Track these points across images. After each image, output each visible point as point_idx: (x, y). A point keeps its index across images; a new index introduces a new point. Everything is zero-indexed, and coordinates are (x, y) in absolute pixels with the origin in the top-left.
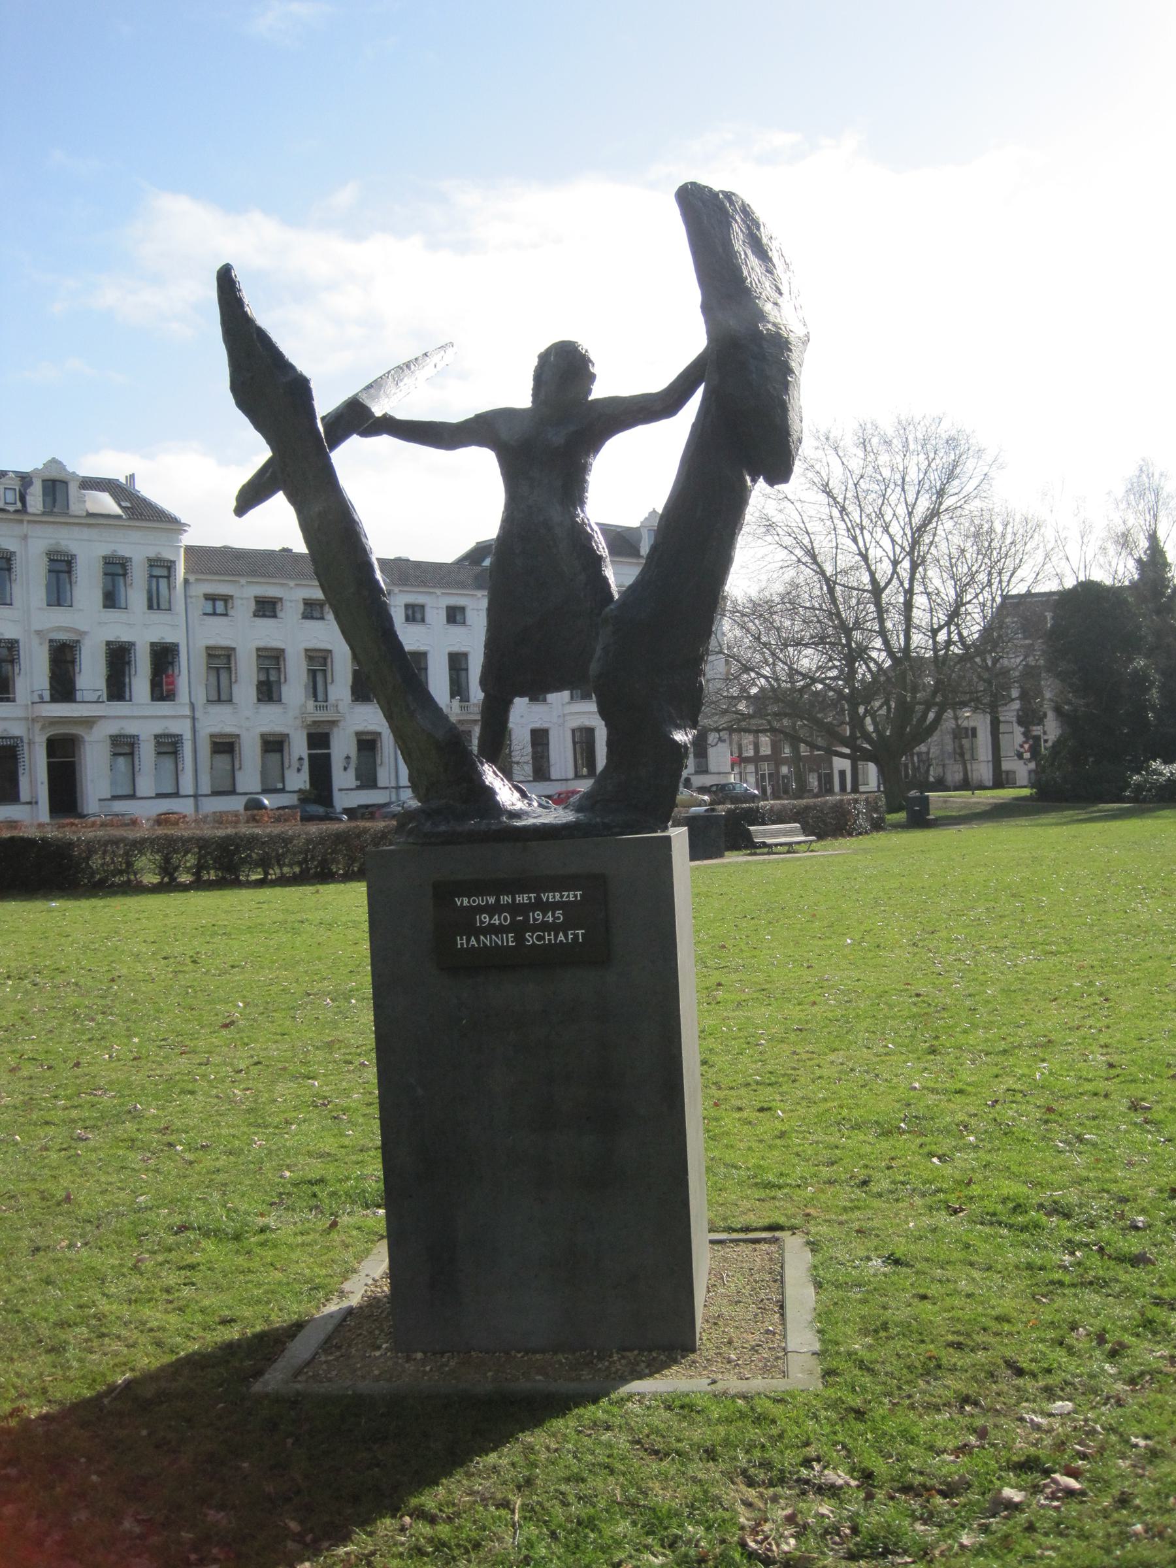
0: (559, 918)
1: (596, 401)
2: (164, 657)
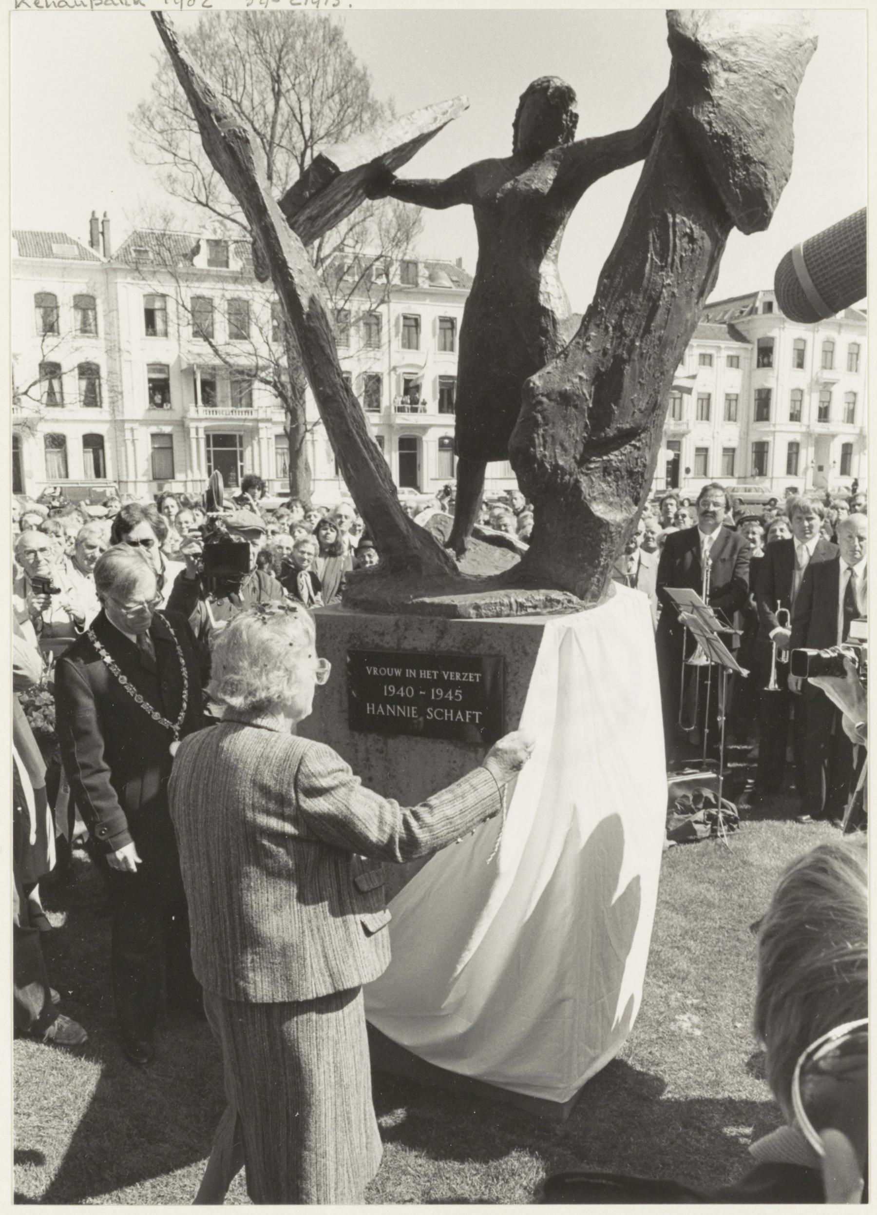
0: (458, 697)
1: (581, 143)
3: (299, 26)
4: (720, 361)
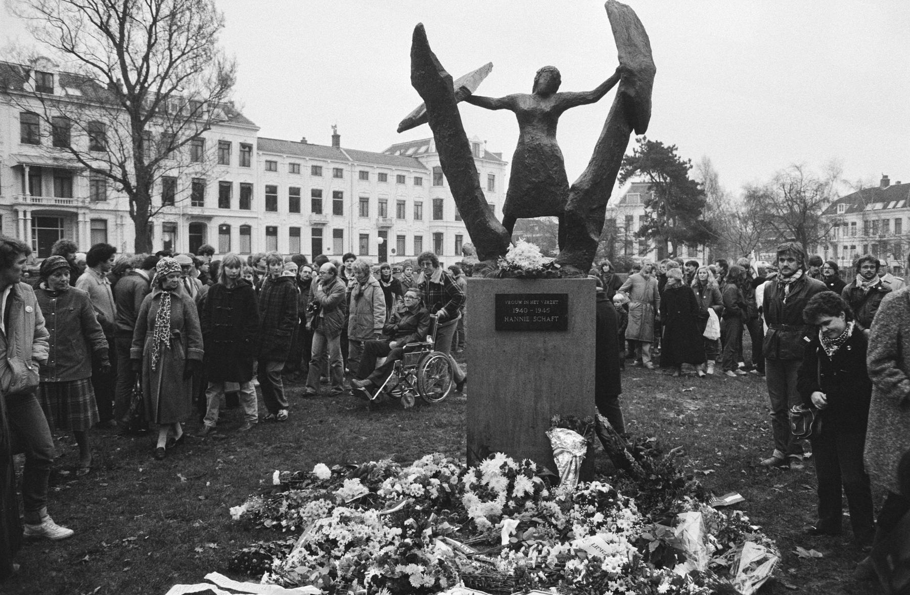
2: (246, 191)
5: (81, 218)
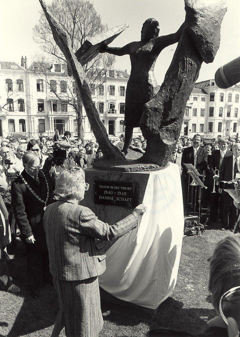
3: (81, 4)
4: (199, 99)
5: (70, 119)
